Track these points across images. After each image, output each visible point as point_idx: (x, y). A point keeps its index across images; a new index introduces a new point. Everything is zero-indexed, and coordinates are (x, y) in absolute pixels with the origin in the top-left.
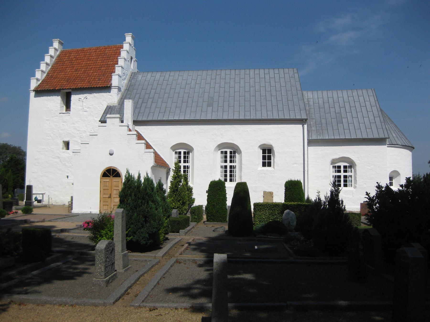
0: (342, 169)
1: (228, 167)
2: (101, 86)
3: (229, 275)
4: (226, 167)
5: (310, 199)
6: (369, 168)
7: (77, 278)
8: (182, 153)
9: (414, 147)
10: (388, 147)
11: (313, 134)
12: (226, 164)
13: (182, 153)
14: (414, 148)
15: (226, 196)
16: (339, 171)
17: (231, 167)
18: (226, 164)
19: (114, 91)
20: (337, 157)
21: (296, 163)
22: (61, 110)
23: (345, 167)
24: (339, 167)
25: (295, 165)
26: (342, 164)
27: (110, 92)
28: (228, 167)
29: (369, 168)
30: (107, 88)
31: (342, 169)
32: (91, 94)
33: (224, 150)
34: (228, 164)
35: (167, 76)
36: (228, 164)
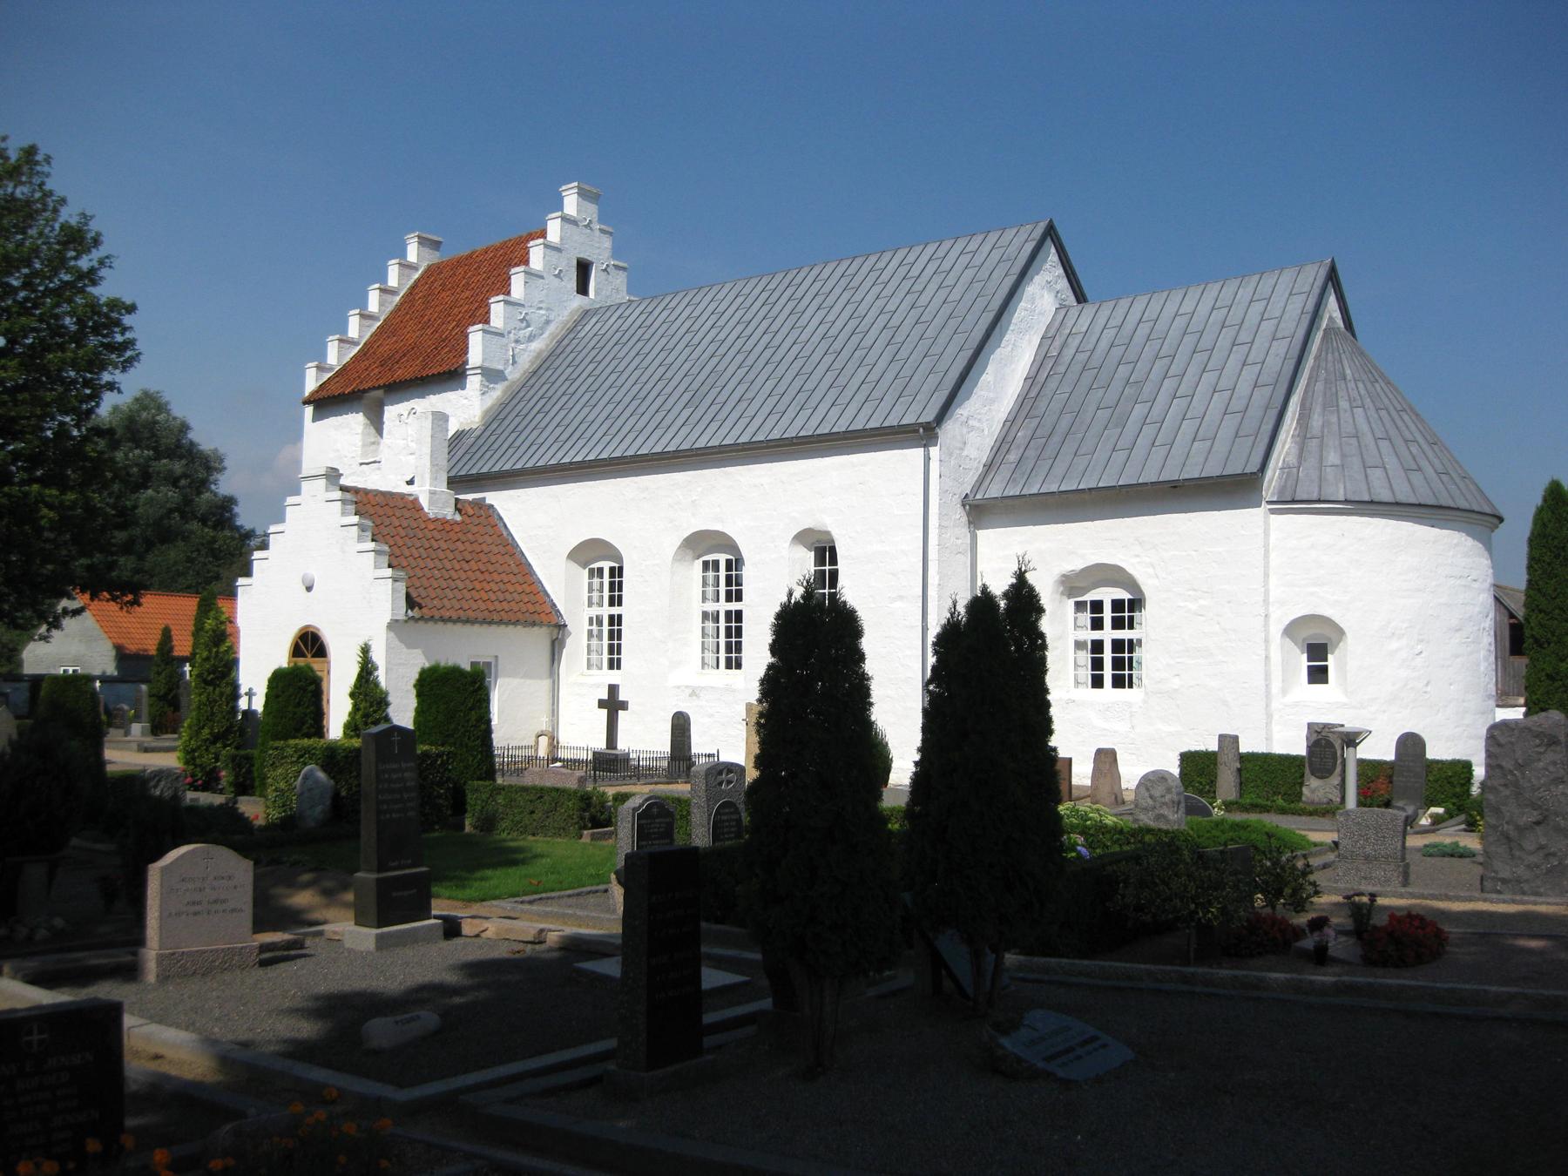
0: (1107, 615)
1: (1108, 647)
2: (441, 370)
3: (605, 979)
4: (1097, 646)
5: (132, 647)
6: (1193, 607)
7: (451, 978)
8: (1107, 608)
9: (1503, 512)
10: (1273, 512)
11: (997, 478)
12: (1097, 635)
13: (1107, 608)
14: (1501, 520)
15: (924, 741)
16: (1097, 624)
17: (1118, 645)
18: (1097, 635)
19: (474, 382)
20: (1078, 565)
21: (901, 598)
22: (364, 454)
23: (1117, 605)
24: (1097, 606)
25: (898, 604)
26: (1107, 595)
27: (463, 388)
28: (1108, 647)
29: (1193, 607)
30: (453, 376)
31: (1107, 615)
32: (423, 397)
33: (710, 557)
34: (1108, 635)
35: (1245, 293)
36: (1108, 635)
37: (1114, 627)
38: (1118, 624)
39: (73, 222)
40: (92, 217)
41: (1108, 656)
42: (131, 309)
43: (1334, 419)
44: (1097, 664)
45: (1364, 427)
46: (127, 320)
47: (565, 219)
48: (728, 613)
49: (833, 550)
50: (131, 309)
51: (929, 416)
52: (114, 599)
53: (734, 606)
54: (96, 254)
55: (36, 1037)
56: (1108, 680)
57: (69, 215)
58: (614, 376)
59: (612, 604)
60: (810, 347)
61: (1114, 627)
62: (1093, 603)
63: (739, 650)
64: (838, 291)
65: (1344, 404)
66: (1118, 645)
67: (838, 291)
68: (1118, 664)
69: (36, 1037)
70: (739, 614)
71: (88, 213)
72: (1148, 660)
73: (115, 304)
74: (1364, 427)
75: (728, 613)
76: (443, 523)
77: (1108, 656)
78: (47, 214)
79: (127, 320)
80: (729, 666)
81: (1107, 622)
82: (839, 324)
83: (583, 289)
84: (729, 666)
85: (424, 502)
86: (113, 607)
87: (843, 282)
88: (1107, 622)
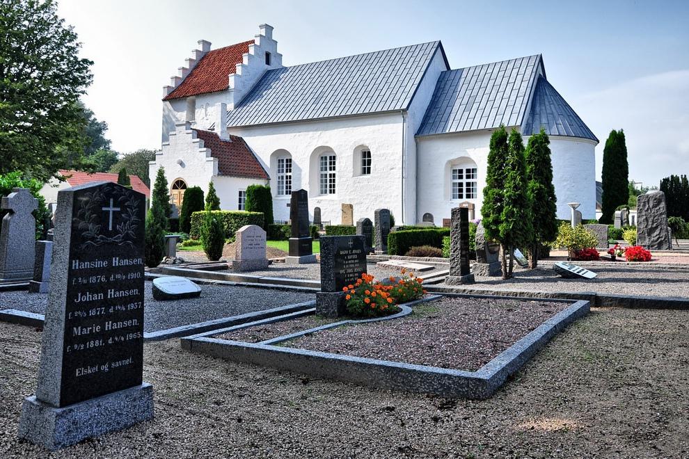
0: (464, 174)
1: (328, 176)
4: (461, 184)
12: (460, 181)
17: (468, 184)
18: (460, 181)
28: (328, 176)
30: (225, 90)
31: (464, 174)
34: (464, 181)
37: (467, 178)
38: (468, 177)
39: (67, 28)
40: (74, 27)
41: (464, 188)
42: (92, 63)
43: (544, 108)
44: (461, 190)
45: (554, 111)
46: (90, 67)
47: (250, 56)
48: (330, 175)
49: (369, 153)
50: (92, 63)
51: (404, 107)
52: (85, 171)
53: (332, 172)
54: (76, 41)
55: (111, 209)
56: (328, 191)
57: (65, 26)
58: (284, 94)
59: (331, 170)
60: (357, 84)
61: (467, 178)
62: (459, 170)
63: (279, 187)
64: (364, 65)
65: (547, 103)
66: (468, 184)
67: (364, 65)
68: (468, 190)
69: (111, 209)
70: (334, 175)
71: (72, 26)
72: (336, 191)
73: (85, 61)
74: (554, 111)
75: (330, 175)
76: (226, 142)
77: (464, 188)
78: (56, 25)
79: (90, 67)
80: (331, 192)
81: (464, 177)
82: (367, 76)
83: (268, 62)
84: (331, 192)
85: (219, 134)
86: (85, 174)
87: (366, 62)
88: (464, 177)
